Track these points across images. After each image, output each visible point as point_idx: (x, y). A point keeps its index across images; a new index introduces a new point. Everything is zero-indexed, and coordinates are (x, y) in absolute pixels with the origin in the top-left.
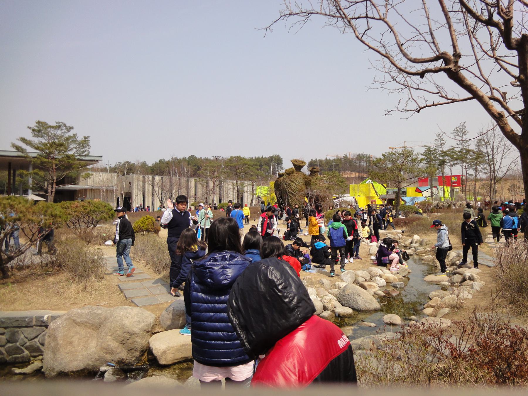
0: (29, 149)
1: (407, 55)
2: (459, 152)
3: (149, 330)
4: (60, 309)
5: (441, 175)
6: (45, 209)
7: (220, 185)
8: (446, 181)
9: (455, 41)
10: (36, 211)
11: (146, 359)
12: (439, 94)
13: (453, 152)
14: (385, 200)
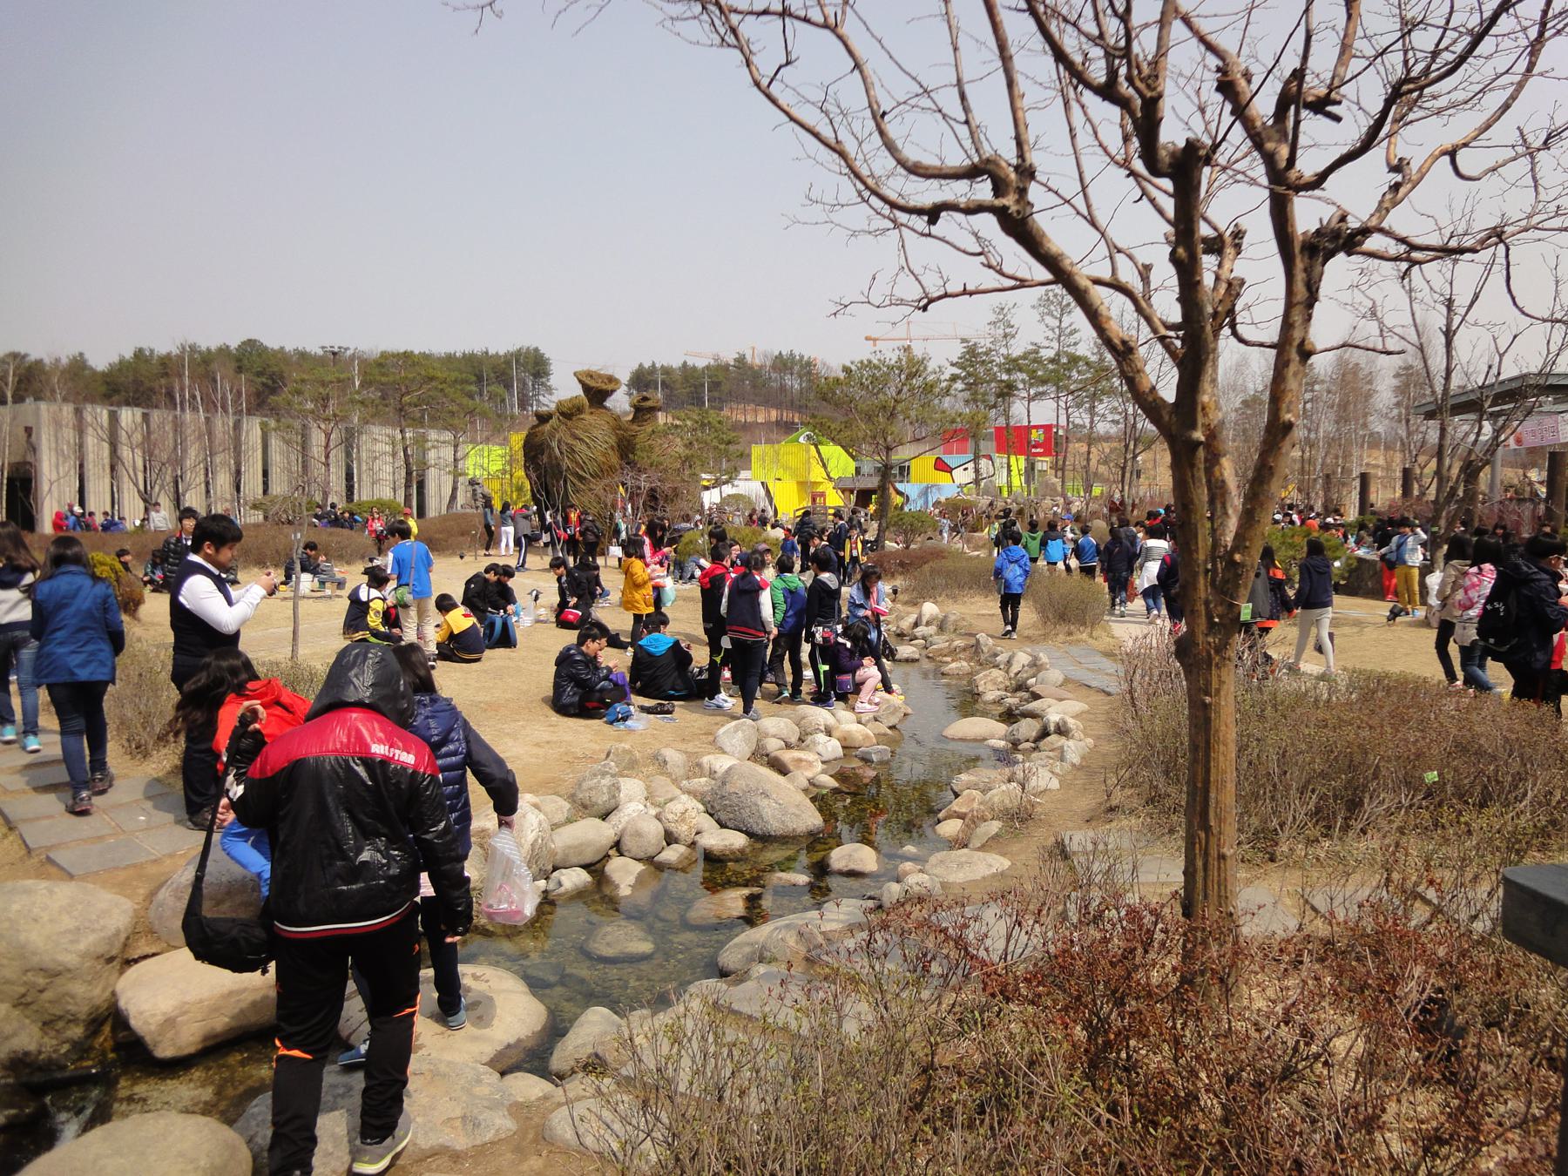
1: (897, 149)
2: (1052, 361)
3: (114, 952)
5: (1001, 422)
7: (349, 443)
8: (1015, 440)
9: (1022, 127)
11: (109, 1044)
12: (982, 258)
13: (1035, 361)
14: (852, 492)
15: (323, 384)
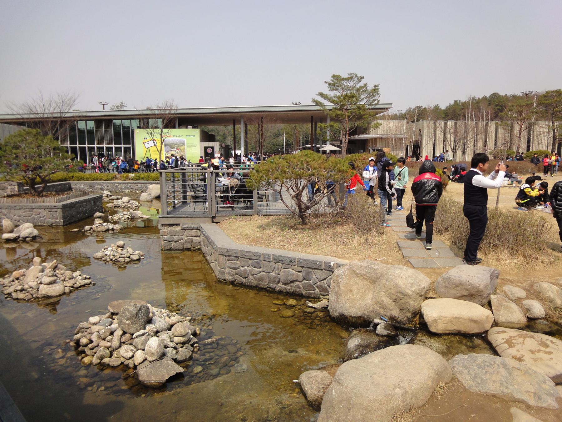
0: (326, 102)
4: (344, 258)
6: (334, 165)
7: (530, 129)
10: (327, 167)
11: (417, 322)
15: (521, 106)
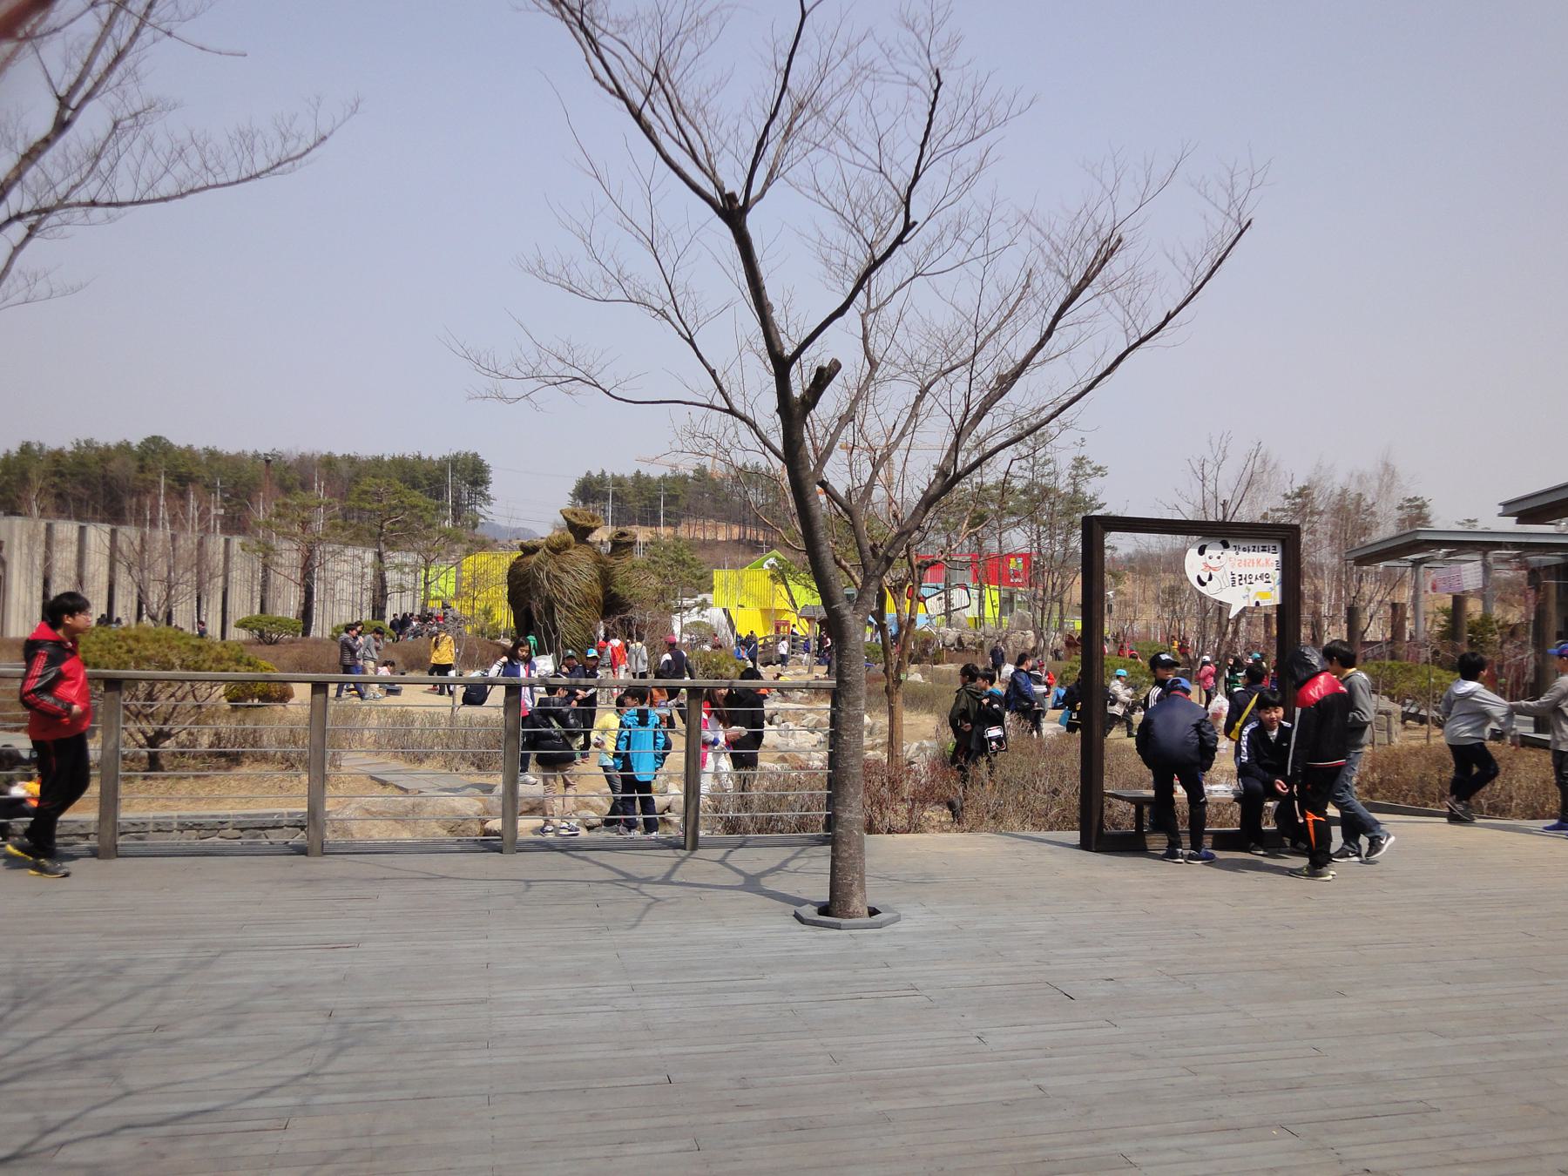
2: (1024, 492)
